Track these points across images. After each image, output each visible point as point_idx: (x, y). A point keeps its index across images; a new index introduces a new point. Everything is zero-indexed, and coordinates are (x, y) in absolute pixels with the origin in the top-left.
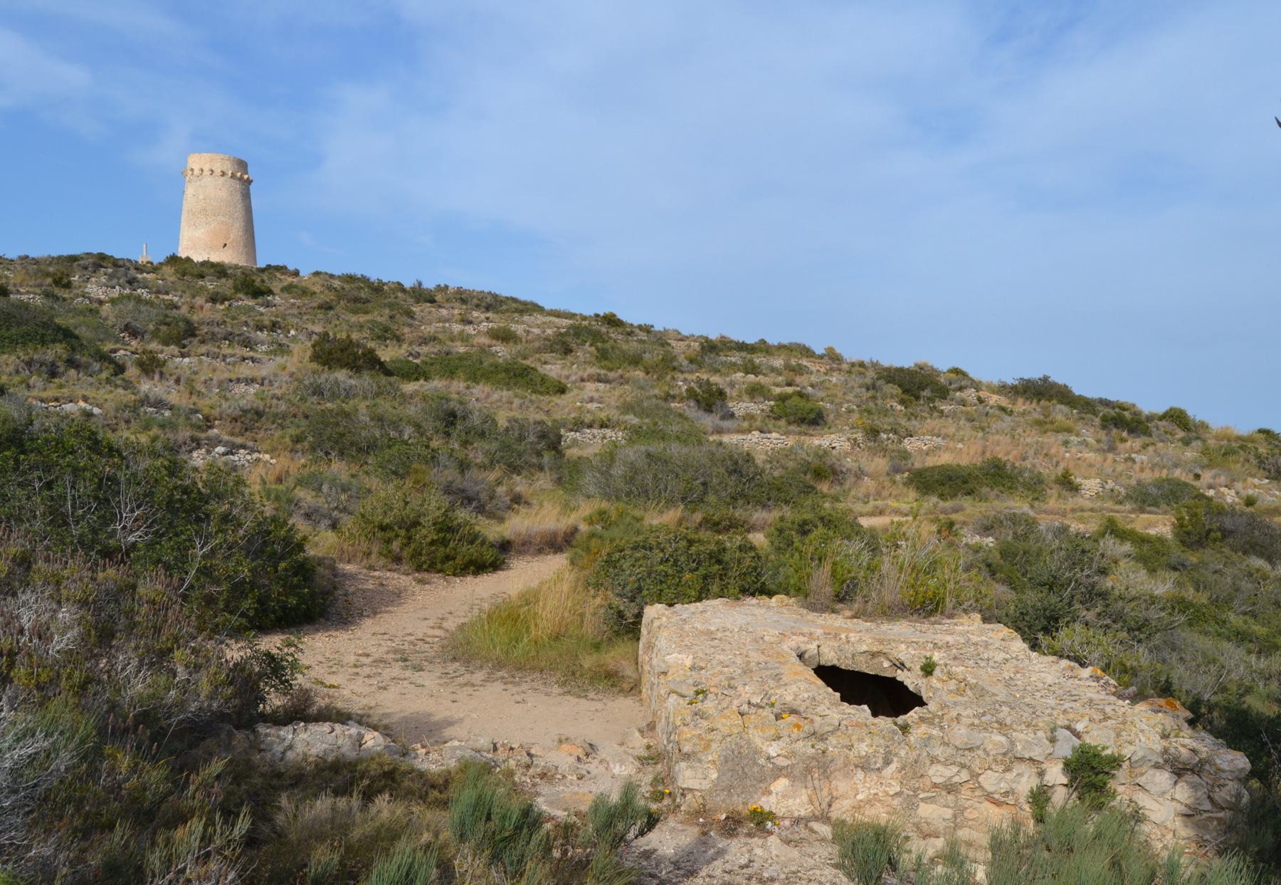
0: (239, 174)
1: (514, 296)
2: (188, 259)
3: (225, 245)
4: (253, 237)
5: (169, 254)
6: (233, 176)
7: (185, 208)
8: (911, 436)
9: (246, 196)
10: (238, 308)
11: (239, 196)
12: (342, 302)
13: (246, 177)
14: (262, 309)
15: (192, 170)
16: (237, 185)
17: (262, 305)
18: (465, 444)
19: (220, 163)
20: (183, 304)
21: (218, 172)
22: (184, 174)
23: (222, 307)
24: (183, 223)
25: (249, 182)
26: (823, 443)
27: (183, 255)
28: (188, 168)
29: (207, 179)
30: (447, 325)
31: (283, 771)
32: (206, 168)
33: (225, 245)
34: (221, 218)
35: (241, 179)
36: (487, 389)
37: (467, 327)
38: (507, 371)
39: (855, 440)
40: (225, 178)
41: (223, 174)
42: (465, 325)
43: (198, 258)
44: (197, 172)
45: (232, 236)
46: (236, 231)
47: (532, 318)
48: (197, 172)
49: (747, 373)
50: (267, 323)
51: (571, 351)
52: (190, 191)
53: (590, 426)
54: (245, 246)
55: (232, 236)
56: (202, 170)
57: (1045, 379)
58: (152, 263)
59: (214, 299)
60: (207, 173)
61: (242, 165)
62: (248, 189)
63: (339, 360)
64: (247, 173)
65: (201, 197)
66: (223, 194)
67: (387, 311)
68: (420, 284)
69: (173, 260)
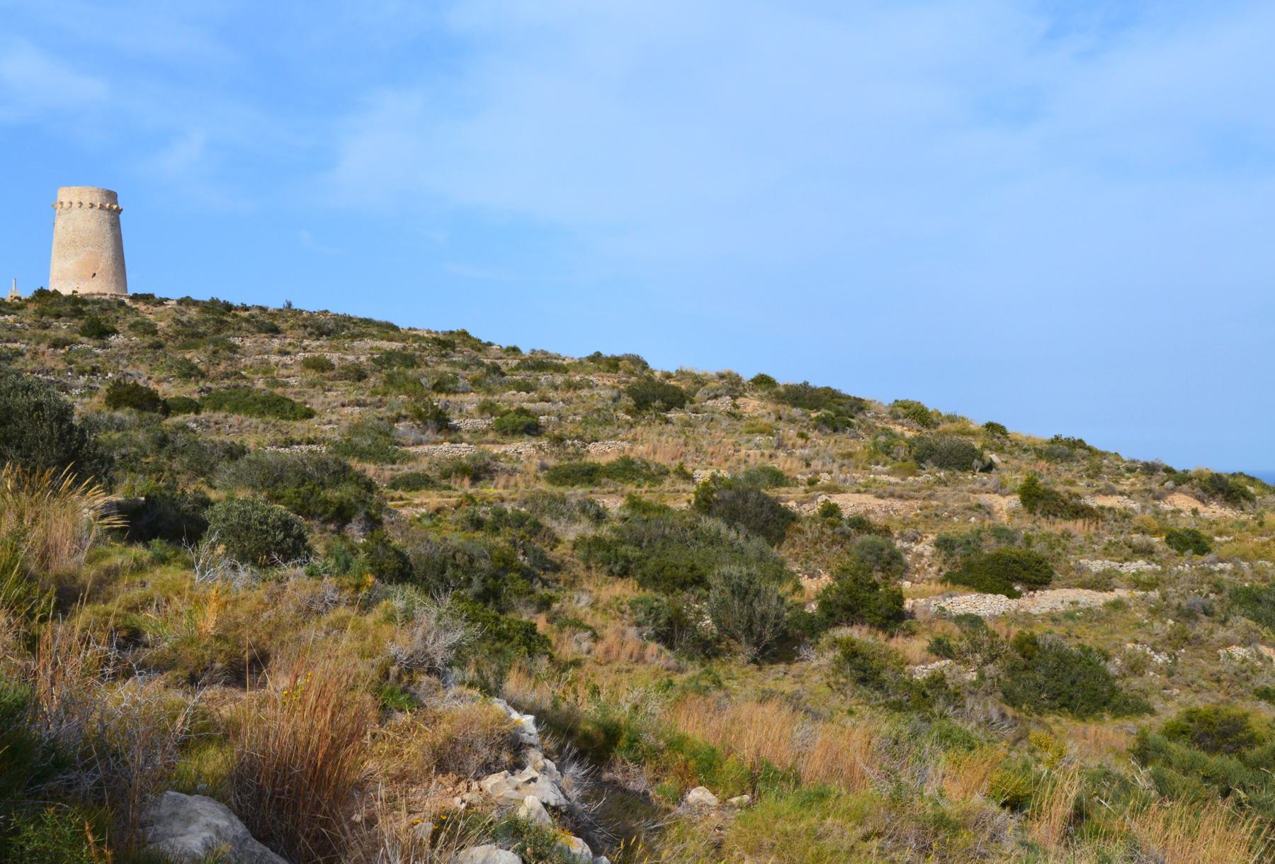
0: (107, 205)
1: (367, 316)
2: (56, 292)
3: (94, 275)
4: (123, 265)
5: (37, 287)
6: (102, 207)
7: (56, 239)
8: (597, 441)
9: (116, 225)
10: (77, 351)
11: (107, 226)
12: (180, 338)
13: (115, 207)
14: (99, 351)
15: (62, 203)
16: (106, 216)
17: (99, 347)
18: (170, 458)
19: (90, 195)
20: (28, 351)
21: (86, 204)
22: (54, 207)
23: (62, 351)
24: (53, 254)
25: (119, 211)
26: (508, 449)
27: (51, 289)
28: (58, 201)
29: (76, 212)
30: (266, 357)
31: (190, 828)
32: (75, 201)
33: (94, 275)
34: (89, 249)
35: (110, 209)
36: (242, 417)
37: (284, 358)
38: (263, 402)
39: (540, 447)
40: (93, 209)
41: (92, 206)
42: (282, 356)
43: (66, 291)
44: (66, 205)
45: (101, 265)
46: (105, 260)
47: (362, 343)
48: (66, 205)
49: (519, 391)
50: (88, 368)
51: (365, 377)
52: (59, 223)
53: (299, 443)
54: (115, 274)
55: (101, 265)
56: (71, 203)
57: (806, 384)
58: (19, 299)
59: (56, 344)
60: (76, 205)
61: (112, 196)
62: (118, 219)
63: (125, 400)
64: (116, 203)
65: (70, 229)
66: (92, 225)
67: (211, 347)
68: (290, 305)
69: (42, 294)
